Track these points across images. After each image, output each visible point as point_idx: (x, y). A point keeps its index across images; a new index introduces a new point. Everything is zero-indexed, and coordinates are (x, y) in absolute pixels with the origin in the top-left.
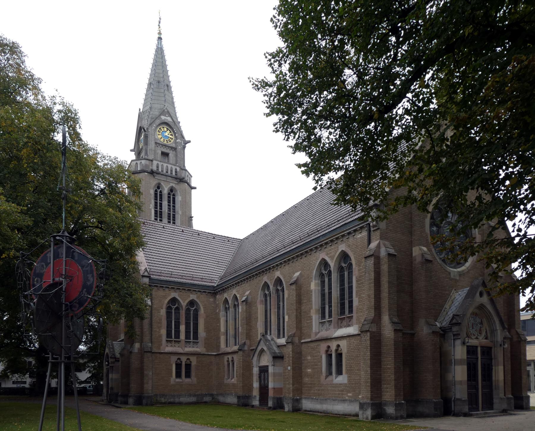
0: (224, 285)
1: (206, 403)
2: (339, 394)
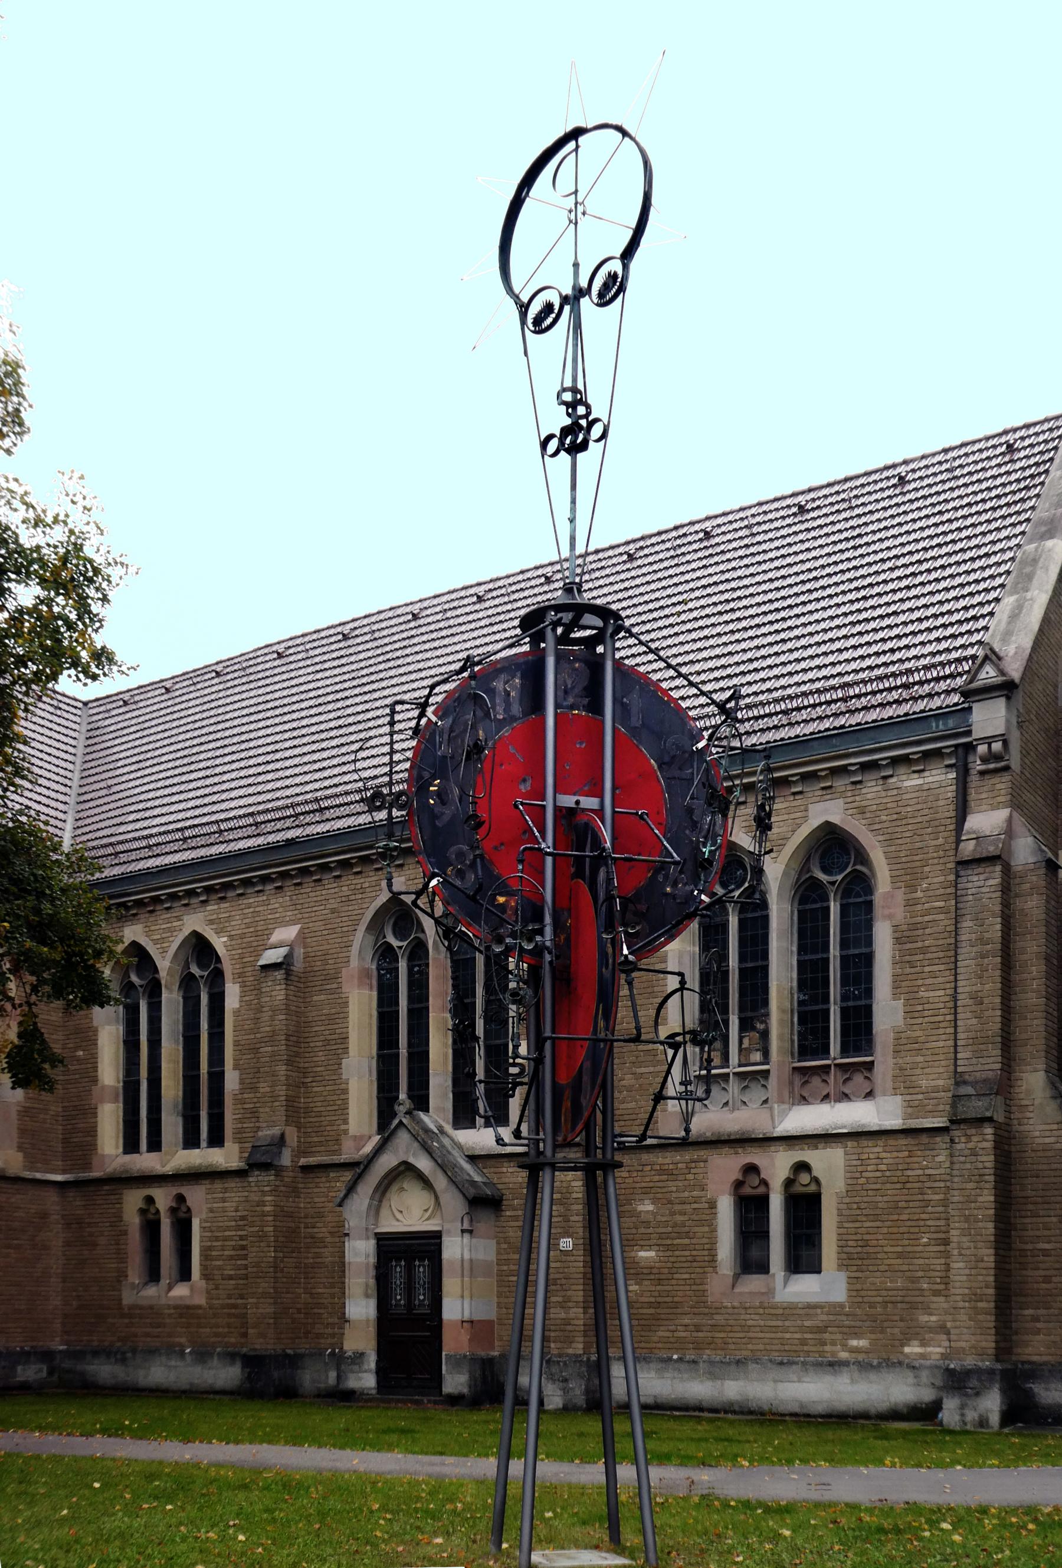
0: (132, 888)
1: (25, 1388)
2: (803, 1342)
